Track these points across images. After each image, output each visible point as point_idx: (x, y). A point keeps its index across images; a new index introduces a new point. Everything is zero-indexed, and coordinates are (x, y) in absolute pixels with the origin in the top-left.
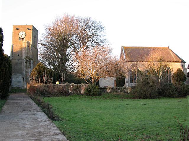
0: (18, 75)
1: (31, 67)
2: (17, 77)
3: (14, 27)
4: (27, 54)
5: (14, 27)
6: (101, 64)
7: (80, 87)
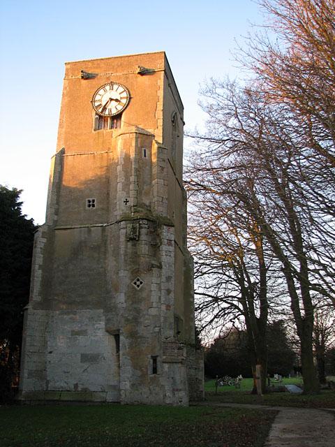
0: (85, 314)
1: (160, 267)
3: (72, 67)
4: (139, 193)
5: (72, 67)
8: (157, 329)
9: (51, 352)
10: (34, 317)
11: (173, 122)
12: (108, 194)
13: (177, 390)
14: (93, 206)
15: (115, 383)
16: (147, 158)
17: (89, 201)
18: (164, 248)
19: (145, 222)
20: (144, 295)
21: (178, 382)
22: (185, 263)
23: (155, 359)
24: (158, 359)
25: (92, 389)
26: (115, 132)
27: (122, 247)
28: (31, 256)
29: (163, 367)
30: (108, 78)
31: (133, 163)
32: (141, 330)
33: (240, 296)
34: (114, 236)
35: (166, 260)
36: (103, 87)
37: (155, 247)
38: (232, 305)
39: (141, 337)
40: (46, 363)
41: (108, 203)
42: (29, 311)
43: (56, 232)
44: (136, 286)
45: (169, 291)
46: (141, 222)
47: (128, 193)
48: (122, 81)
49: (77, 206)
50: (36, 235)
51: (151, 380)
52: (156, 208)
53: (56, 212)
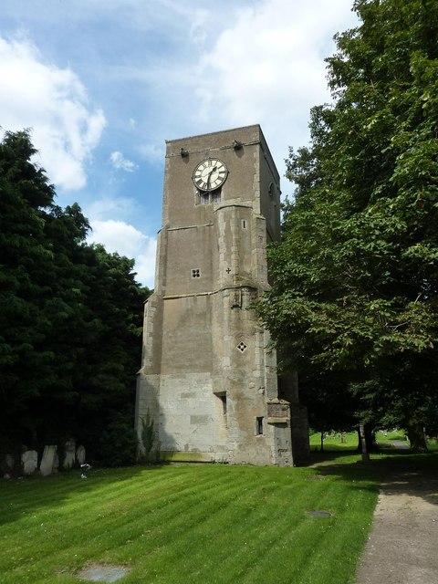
0: (193, 377)
14: (198, 276)
20: (248, 358)
21: (283, 442)
23: (260, 420)
30: (207, 154)
32: (247, 392)
36: (201, 163)
41: (211, 273)
43: (165, 301)
47: (230, 263)
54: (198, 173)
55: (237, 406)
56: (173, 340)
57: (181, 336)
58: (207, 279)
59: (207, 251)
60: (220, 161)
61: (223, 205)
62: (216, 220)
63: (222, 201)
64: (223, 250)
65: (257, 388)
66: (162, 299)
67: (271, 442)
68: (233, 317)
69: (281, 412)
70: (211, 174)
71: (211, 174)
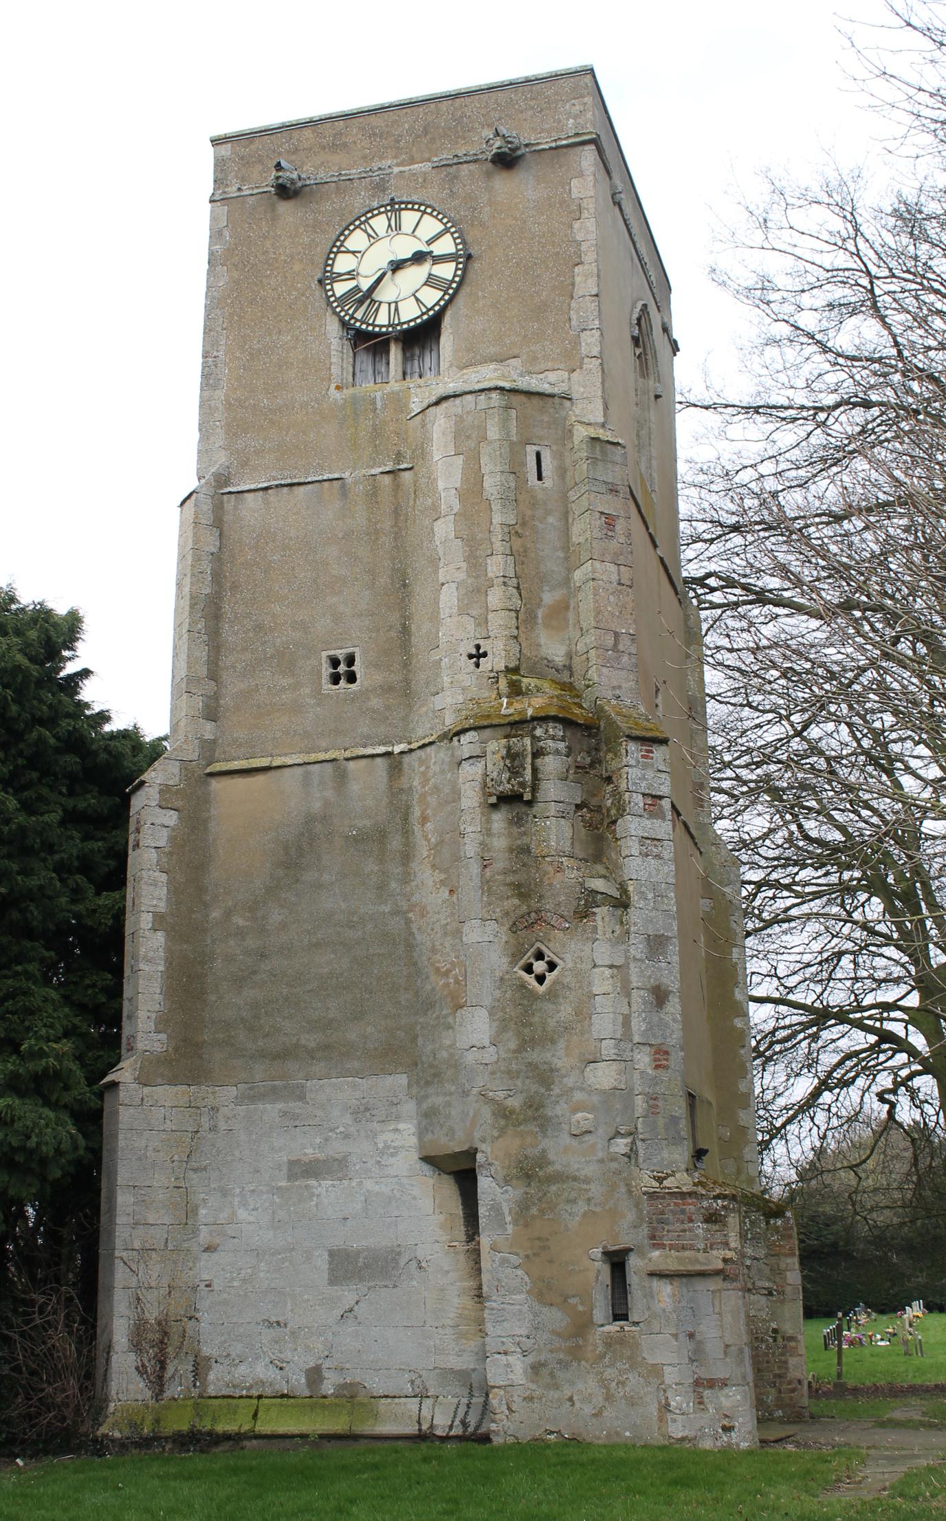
0: (336, 1094)
1: (622, 903)
2: (308, 1147)
3: (236, 151)
4: (524, 618)
5: (236, 151)
6: (930, 608)
7: (664, 819)
8: (621, 1145)
9: (209, 1249)
10: (145, 1116)
11: (636, 341)
12: (405, 631)
13: (711, 1384)
14: (352, 678)
15: (464, 1362)
16: (548, 482)
17: (335, 662)
18: (633, 827)
19: (556, 730)
20: (565, 1011)
21: (713, 1348)
22: (707, 886)
23: (617, 1262)
24: (633, 1262)
25: (376, 1384)
26: (419, 394)
27: (471, 827)
28: (122, 883)
29: (650, 1295)
30: (381, 187)
31: (496, 507)
32: (562, 1152)
33: (913, 1000)
34: (436, 789)
35: (643, 876)
36: (360, 220)
37: (598, 825)
38: (886, 1037)
39: (559, 1178)
40: (195, 1289)
41: (406, 665)
42: (123, 1094)
43: (215, 784)
44: (530, 980)
45: (659, 996)
46: (539, 732)
47: (482, 621)
48: (431, 194)
49: (285, 682)
50: (137, 802)
51: (608, 1345)
52: (592, 673)
53: (206, 706)
54: (343, 264)
55: (523, 1207)
56: (251, 942)
57: (283, 926)
58: (388, 689)
59: (384, 580)
60: (436, 213)
61: (452, 387)
62: (422, 452)
63: (448, 368)
64: (451, 573)
65: (603, 1132)
66: (206, 773)
67: (664, 1352)
68: (499, 844)
69: (700, 1228)
70: (397, 266)
71: (397, 266)
